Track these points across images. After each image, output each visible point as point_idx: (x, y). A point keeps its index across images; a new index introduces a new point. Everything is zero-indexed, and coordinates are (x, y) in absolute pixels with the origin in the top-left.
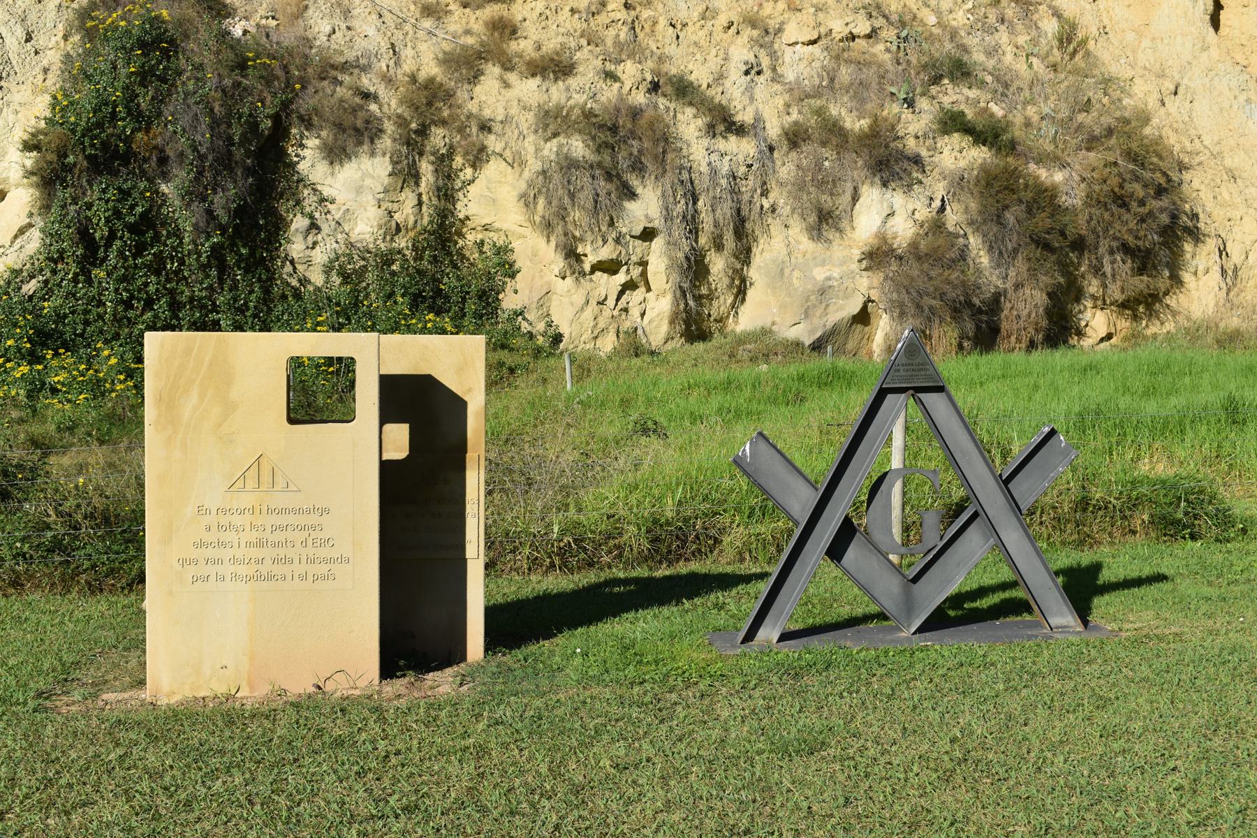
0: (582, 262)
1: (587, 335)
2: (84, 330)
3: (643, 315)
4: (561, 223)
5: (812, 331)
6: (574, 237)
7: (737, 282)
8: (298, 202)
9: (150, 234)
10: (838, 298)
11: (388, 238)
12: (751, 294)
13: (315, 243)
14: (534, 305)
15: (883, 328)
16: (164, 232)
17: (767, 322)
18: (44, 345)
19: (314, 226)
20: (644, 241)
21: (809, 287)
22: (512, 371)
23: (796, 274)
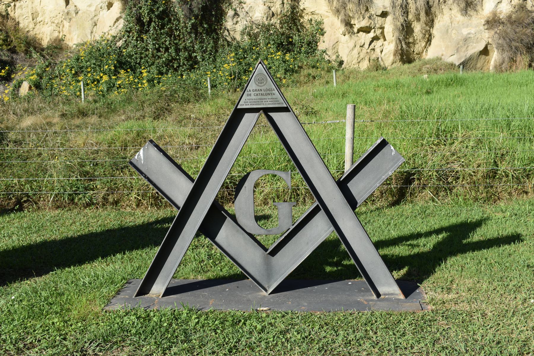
0: (353, 27)
1: (355, 61)
2: (140, 61)
3: (382, 52)
4: (343, 10)
5: (460, 59)
6: (350, 16)
7: (427, 36)
8: (230, 4)
9: (166, 19)
10: (473, 43)
11: (269, 19)
12: (433, 41)
13: (237, 22)
14: (331, 48)
15: (495, 56)
16: (173, 19)
17: (439, 54)
18: (121, 68)
19: (236, 14)
20: (383, 17)
21: (460, 38)
22: (314, 78)
23: (454, 31)
